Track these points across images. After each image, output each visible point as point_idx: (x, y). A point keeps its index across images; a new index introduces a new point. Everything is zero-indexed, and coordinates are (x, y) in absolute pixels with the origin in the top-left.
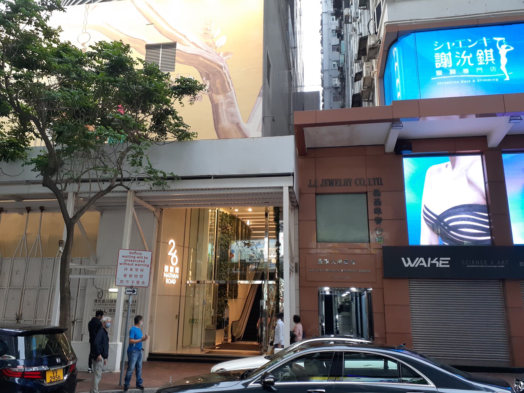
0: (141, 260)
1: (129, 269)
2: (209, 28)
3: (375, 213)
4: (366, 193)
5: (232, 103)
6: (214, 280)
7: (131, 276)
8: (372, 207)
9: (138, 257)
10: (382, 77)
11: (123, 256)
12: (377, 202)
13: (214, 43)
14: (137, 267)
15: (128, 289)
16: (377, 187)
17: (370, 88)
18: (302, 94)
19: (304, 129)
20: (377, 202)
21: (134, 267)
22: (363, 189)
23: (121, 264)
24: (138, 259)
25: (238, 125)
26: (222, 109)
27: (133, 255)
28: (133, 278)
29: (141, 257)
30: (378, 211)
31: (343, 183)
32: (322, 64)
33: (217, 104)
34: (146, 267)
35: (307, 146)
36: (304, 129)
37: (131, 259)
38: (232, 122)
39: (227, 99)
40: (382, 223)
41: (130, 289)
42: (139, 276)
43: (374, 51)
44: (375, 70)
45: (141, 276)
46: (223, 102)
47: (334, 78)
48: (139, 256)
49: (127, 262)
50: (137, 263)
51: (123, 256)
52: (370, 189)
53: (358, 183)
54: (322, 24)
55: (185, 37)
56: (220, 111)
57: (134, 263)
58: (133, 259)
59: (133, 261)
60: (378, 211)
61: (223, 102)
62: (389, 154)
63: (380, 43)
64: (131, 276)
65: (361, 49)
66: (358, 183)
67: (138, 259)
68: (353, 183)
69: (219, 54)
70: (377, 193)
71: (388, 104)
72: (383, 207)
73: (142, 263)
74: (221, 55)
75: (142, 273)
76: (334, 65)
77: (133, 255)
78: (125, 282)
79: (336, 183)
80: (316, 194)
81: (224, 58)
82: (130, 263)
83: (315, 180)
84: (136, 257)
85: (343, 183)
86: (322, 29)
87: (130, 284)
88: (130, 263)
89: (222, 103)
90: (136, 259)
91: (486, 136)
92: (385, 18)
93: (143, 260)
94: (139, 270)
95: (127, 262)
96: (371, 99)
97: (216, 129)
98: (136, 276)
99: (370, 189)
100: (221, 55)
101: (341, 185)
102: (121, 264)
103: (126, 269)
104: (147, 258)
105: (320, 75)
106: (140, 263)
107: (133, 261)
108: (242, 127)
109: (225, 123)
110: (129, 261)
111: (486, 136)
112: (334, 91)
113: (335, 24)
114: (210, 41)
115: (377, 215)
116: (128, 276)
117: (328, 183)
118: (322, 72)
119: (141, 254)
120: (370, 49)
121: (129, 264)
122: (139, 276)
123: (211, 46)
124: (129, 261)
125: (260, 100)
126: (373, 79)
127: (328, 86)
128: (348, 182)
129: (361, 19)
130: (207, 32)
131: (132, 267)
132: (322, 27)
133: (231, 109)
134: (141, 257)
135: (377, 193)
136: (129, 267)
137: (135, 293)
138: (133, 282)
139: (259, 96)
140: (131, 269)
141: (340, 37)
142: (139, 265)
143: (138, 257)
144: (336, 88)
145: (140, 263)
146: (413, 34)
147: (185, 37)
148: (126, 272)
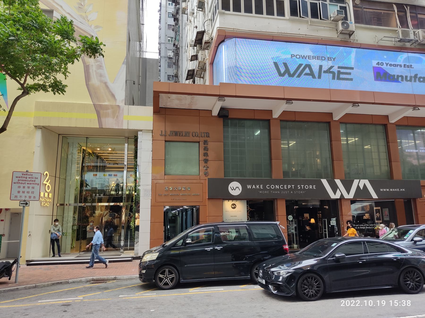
0: (32, 179)
1: (22, 187)
2: (83, 4)
3: (204, 156)
4: (199, 142)
5: (101, 66)
6: (293, 234)
7: (23, 192)
8: (202, 152)
9: (29, 178)
10: (212, 63)
11: (17, 177)
12: (206, 149)
13: (87, 17)
14: (29, 185)
15: (21, 202)
16: (206, 139)
17: (203, 69)
18: (146, 59)
19: (160, 94)
20: (206, 149)
21: (26, 185)
22: (197, 139)
23: (15, 183)
24: (30, 179)
25: (105, 83)
26: (93, 70)
27: (25, 176)
28: (26, 194)
29: (32, 178)
30: (206, 155)
31: (184, 134)
32: (160, 38)
33: (88, 65)
34: (37, 185)
35: (160, 106)
36: (160, 94)
37: (23, 179)
38: (101, 81)
39: (96, 62)
40: (209, 162)
41: (23, 202)
42: (30, 192)
43: (208, 45)
44: (207, 57)
45: (33, 192)
46: (94, 64)
47: (169, 50)
48: (30, 176)
49: (21, 182)
50: (29, 182)
51: (17, 177)
52: (202, 139)
53: (194, 135)
54: (160, 6)
55: (61, 7)
56: (91, 71)
57: (26, 182)
58: (25, 179)
59: (26, 180)
60: (206, 155)
61: (94, 64)
62: (215, 116)
63: (212, 40)
64: (28, 192)
65: (197, 39)
66: (194, 135)
67: (30, 179)
68: (191, 135)
69: (91, 26)
70: (205, 142)
71: (216, 83)
72: (209, 152)
73: (33, 182)
74: (93, 27)
75: (33, 190)
76: (169, 40)
77: (25, 176)
78: (18, 197)
79: (180, 134)
80: (165, 141)
81: (95, 30)
82: (23, 182)
83: (165, 131)
84: (28, 178)
85: (184, 134)
86: (160, 10)
87: (23, 199)
88: (23, 182)
89: (92, 65)
90: (28, 179)
91: (271, 111)
92: (217, 25)
93: (34, 180)
94: (31, 188)
95: (21, 182)
96: (202, 76)
97: (87, 85)
98: (28, 192)
99: (202, 139)
100: (93, 27)
101: (182, 136)
102: (15, 183)
103: (19, 187)
104: (37, 178)
105: (157, 46)
106: (31, 182)
107: (26, 180)
108: (109, 86)
109: (95, 81)
110: (22, 180)
111: (271, 111)
112: (168, 60)
113: (172, 9)
114: (84, 14)
115: (205, 158)
116: (21, 192)
117: (174, 134)
118: (160, 44)
119: (32, 175)
120: (206, 43)
121: (21, 183)
122: (30, 192)
123: (84, 18)
124: (22, 180)
125: (124, 68)
126: (205, 64)
127: (164, 55)
128: (187, 134)
129: (197, 15)
130: (81, 7)
131: (24, 185)
132: (161, 8)
133: (100, 71)
134: (32, 178)
135: (205, 142)
136: (22, 186)
137: (28, 205)
138: (26, 197)
139: (123, 63)
140: (24, 187)
141: (176, 21)
142: (30, 184)
143: (29, 178)
144: (170, 58)
145: (31, 182)
146: (234, 39)
147: (61, 7)
148: (19, 190)
